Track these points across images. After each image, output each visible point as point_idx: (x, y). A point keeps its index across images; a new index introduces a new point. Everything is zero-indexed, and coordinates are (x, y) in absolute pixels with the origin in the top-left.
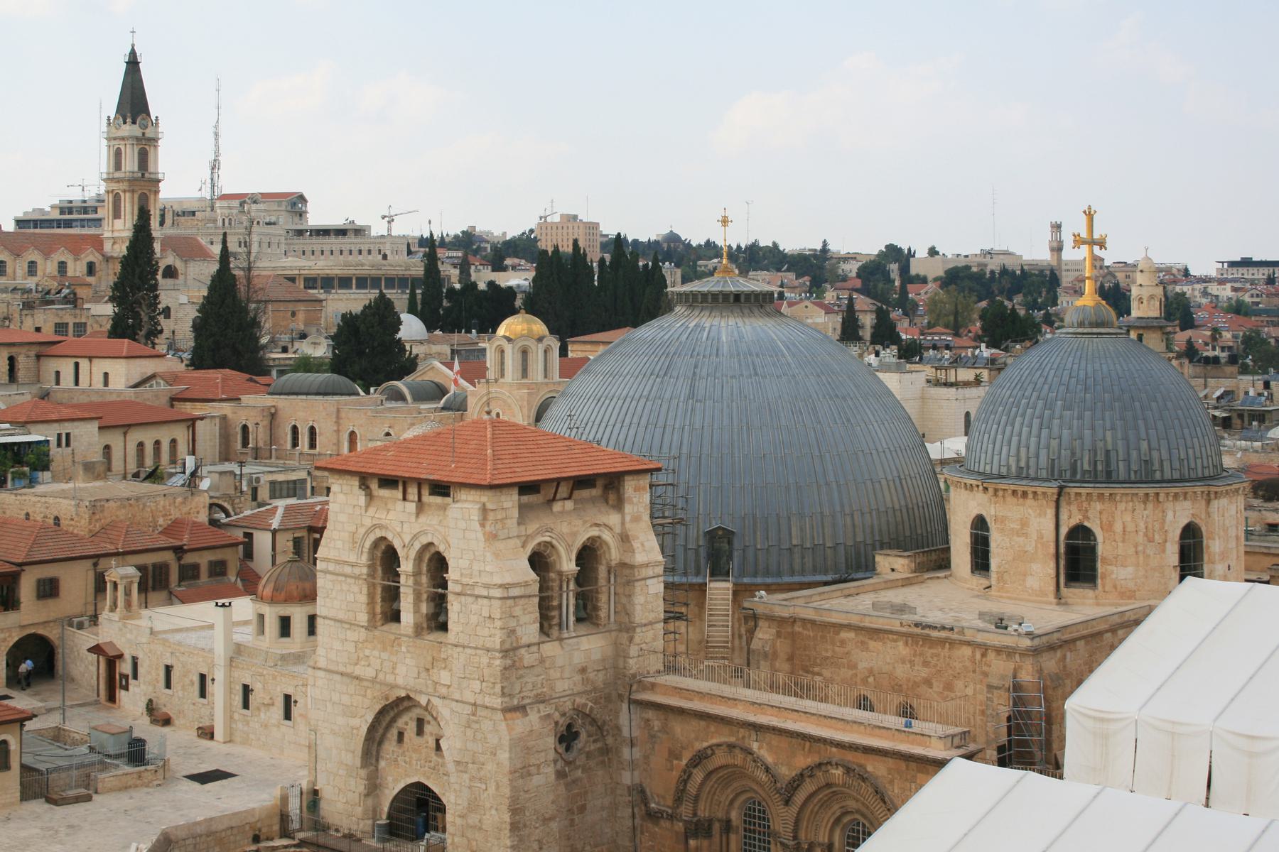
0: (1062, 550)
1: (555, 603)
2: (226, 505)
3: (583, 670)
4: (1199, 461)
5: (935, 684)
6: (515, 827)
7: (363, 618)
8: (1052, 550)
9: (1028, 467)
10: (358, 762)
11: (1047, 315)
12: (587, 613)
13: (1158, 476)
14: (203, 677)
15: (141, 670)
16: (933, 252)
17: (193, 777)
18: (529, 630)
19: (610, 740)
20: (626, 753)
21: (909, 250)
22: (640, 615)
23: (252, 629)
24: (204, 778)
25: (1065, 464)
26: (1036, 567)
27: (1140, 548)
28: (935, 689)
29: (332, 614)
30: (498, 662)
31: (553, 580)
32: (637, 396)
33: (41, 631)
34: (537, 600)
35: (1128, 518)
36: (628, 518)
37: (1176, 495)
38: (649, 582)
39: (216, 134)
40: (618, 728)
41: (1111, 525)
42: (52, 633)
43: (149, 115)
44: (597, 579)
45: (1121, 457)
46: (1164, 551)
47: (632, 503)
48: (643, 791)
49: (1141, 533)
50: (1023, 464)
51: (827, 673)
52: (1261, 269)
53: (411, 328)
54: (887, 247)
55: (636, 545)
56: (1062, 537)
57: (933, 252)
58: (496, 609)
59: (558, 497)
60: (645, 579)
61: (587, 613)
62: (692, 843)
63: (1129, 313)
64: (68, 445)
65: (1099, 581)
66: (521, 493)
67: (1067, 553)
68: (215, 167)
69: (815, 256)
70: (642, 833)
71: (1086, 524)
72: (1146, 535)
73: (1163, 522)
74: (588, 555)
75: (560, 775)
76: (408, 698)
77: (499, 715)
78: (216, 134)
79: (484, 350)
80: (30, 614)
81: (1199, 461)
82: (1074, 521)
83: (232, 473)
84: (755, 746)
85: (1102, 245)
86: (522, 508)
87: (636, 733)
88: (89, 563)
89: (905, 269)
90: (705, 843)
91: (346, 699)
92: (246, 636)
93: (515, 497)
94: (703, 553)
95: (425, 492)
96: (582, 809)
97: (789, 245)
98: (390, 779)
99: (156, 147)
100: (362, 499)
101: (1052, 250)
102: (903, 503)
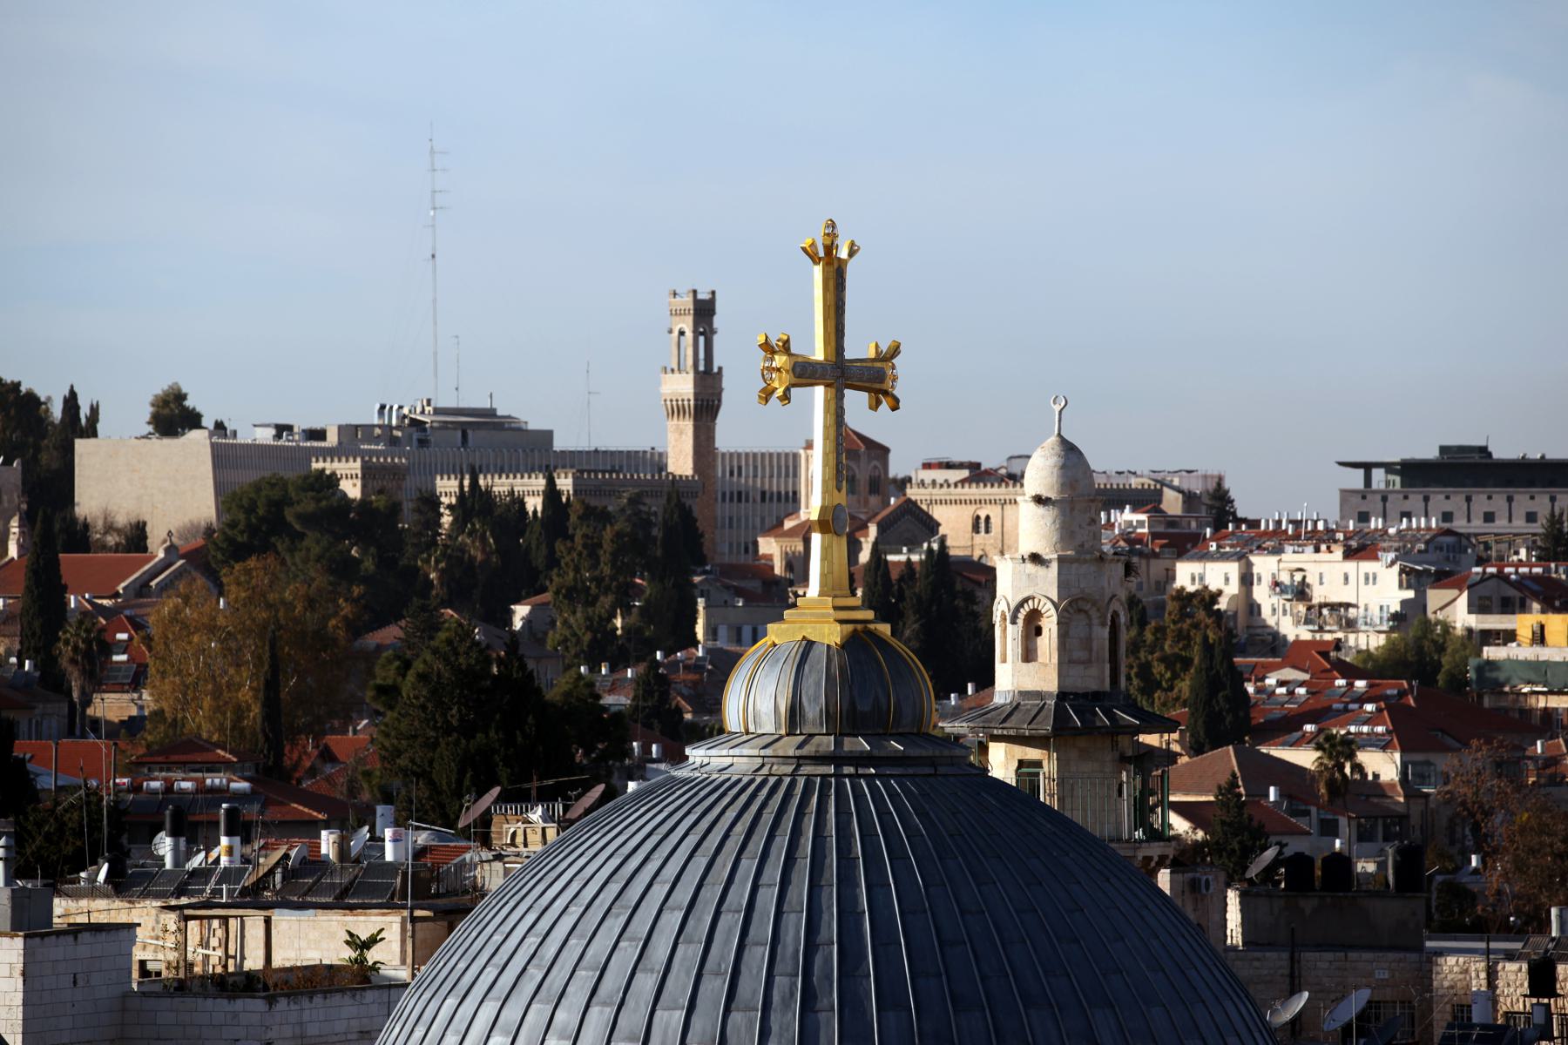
11: (655, 686)
19: (1302, 608)
21: (71, 401)
52: (1524, 501)
63: (986, 679)
66: (1387, 472)
85: (876, 379)
88: (1361, 472)
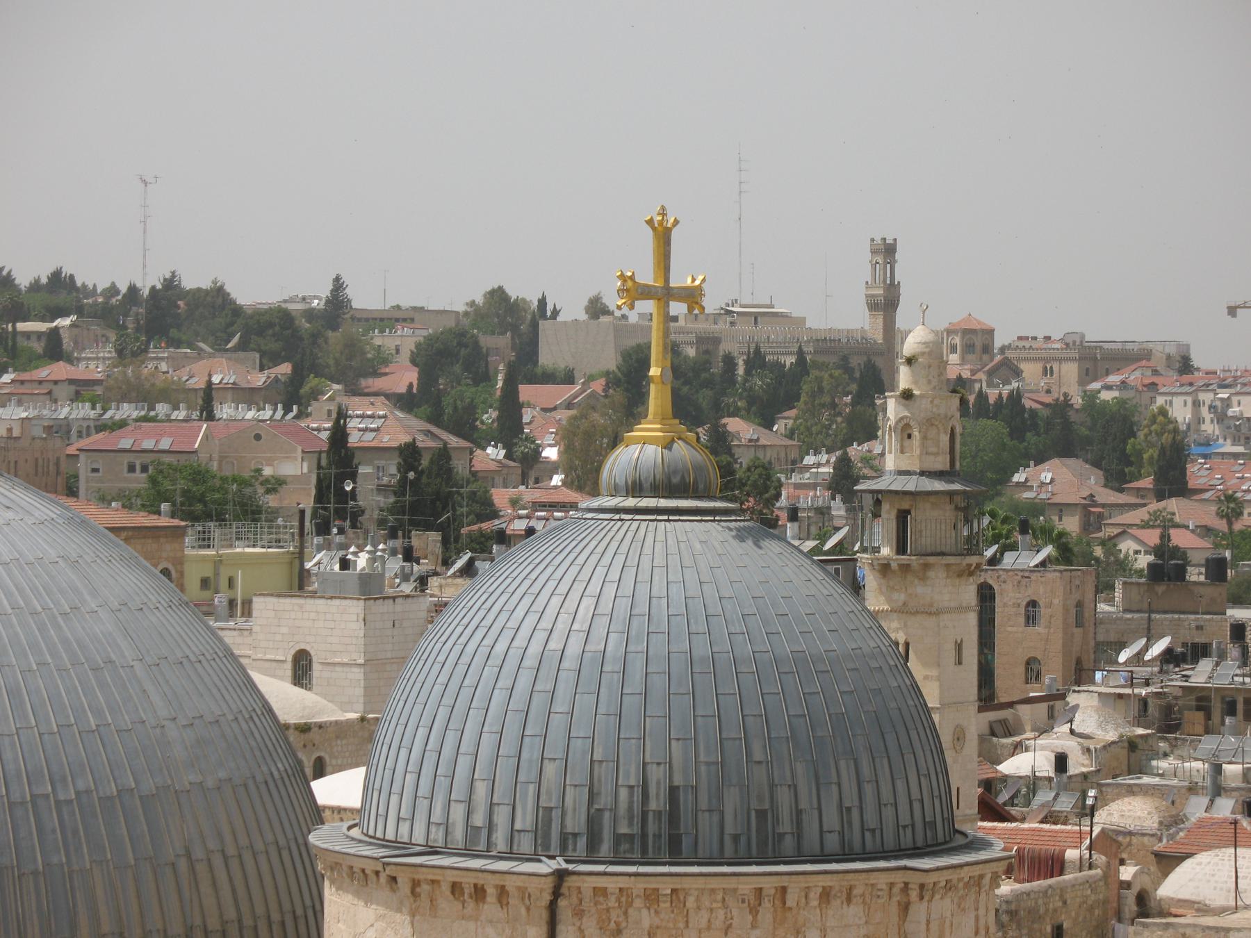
4: (888, 812)
9: (491, 826)
13: (789, 843)
21: (542, 302)
25: (576, 823)
37: (826, 895)
45: (703, 804)
50: (479, 820)
69: (310, 314)
79: (768, 424)
81: (888, 812)
89: (528, 349)
97: (253, 291)
101: (873, 306)
102: (231, 914)
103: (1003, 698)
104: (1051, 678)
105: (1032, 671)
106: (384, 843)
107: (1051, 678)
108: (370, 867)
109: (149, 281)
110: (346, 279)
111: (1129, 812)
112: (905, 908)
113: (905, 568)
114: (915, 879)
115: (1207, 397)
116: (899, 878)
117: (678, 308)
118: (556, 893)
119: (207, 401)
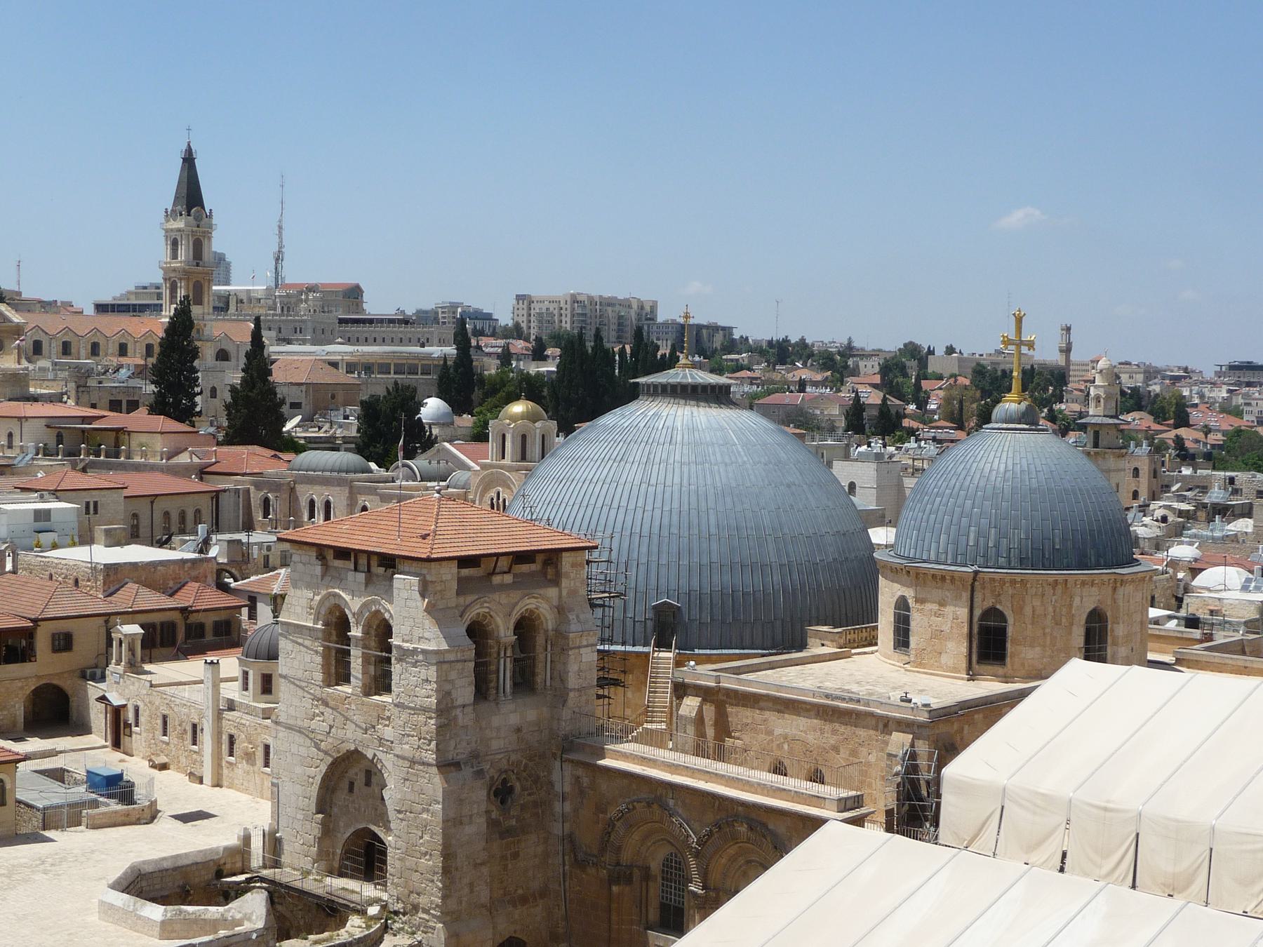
0: (976, 630)
1: (493, 668)
2: (233, 571)
3: (519, 730)
5: (842, 751)
6: (446, 871)
7: (319, 676)
8: (966, 630)
10: (313, 808)
12: (524, 681)
14: (194, 726)
15: (142, 719)
16: (950, 350)
17: (177, 817)
18: (465, 693)
20: (558, 807)
22: (573, 682)
23: (237, 685)
24: (186, 818)
26: (951, 645)
27: (1047, 630)
28: (842, 755)
29: (291, 673)
30: (433, 722)
31: (491, 647)
32: (595, 480)
33: (55, 682)
34: (472, 665)
35: (1037, 603)
36: (564, 593)
38: (583, 651)
39: (280, 227)
40: (551, 784)
41: (1021, 608)
42: (66, 684)
43: (203, 208)
44: (534, 646)
46: (1070, 633)
47: (568, 577)
48: (572, 842)
49: (1049, 617)
51: (747, 738)
53: (432, 407)
54: (905, 345)
55: (572, 617)
56: (976, 619)
57: (950, 350)
58: (432, 673)
59: (497, 570)
60: (579, 647)
61: (524, 681)
62: (615, 889)
64: (96, 512)
65: (1008, 660)
67: (979, 633)
68: (278, 259)
70: (571, 878)
71: (998, 607)
72: (1054, 617)
73: (1071, 605)
74: (525, 627)
75: (493, 824)
76: (356, 751)
77: (435, 770)
78: (280, 227)
80: (45, 666)
82: (988, 603)
83: (239, 541)
84: (671, 803)
86: (461, 580)
87: (567, 789)
90: (627, 889)
91: (303, 751)
92: (232, 691)
93: (455, 570)
94: (650, 624)
95: (374, 562)
96: (516, 856)
98: (342, 824)
99: (210, 238)
100: (318, 569)
103: (208, 496)
104: (1143, 498)
105: (1135, 495)
106: (903, 557)
107: (1143, 498)
108: (899, 567)
109: (781, 337)
110: (854, 339)
111: (1183, 551)
112: (1115, 589)
113: (1096, 453)
114: (1119, 577)
115: (1195, 389)
116: (1113, 577)
117: (1024, 350)
118: (974, 580)
119: (802, 385)
